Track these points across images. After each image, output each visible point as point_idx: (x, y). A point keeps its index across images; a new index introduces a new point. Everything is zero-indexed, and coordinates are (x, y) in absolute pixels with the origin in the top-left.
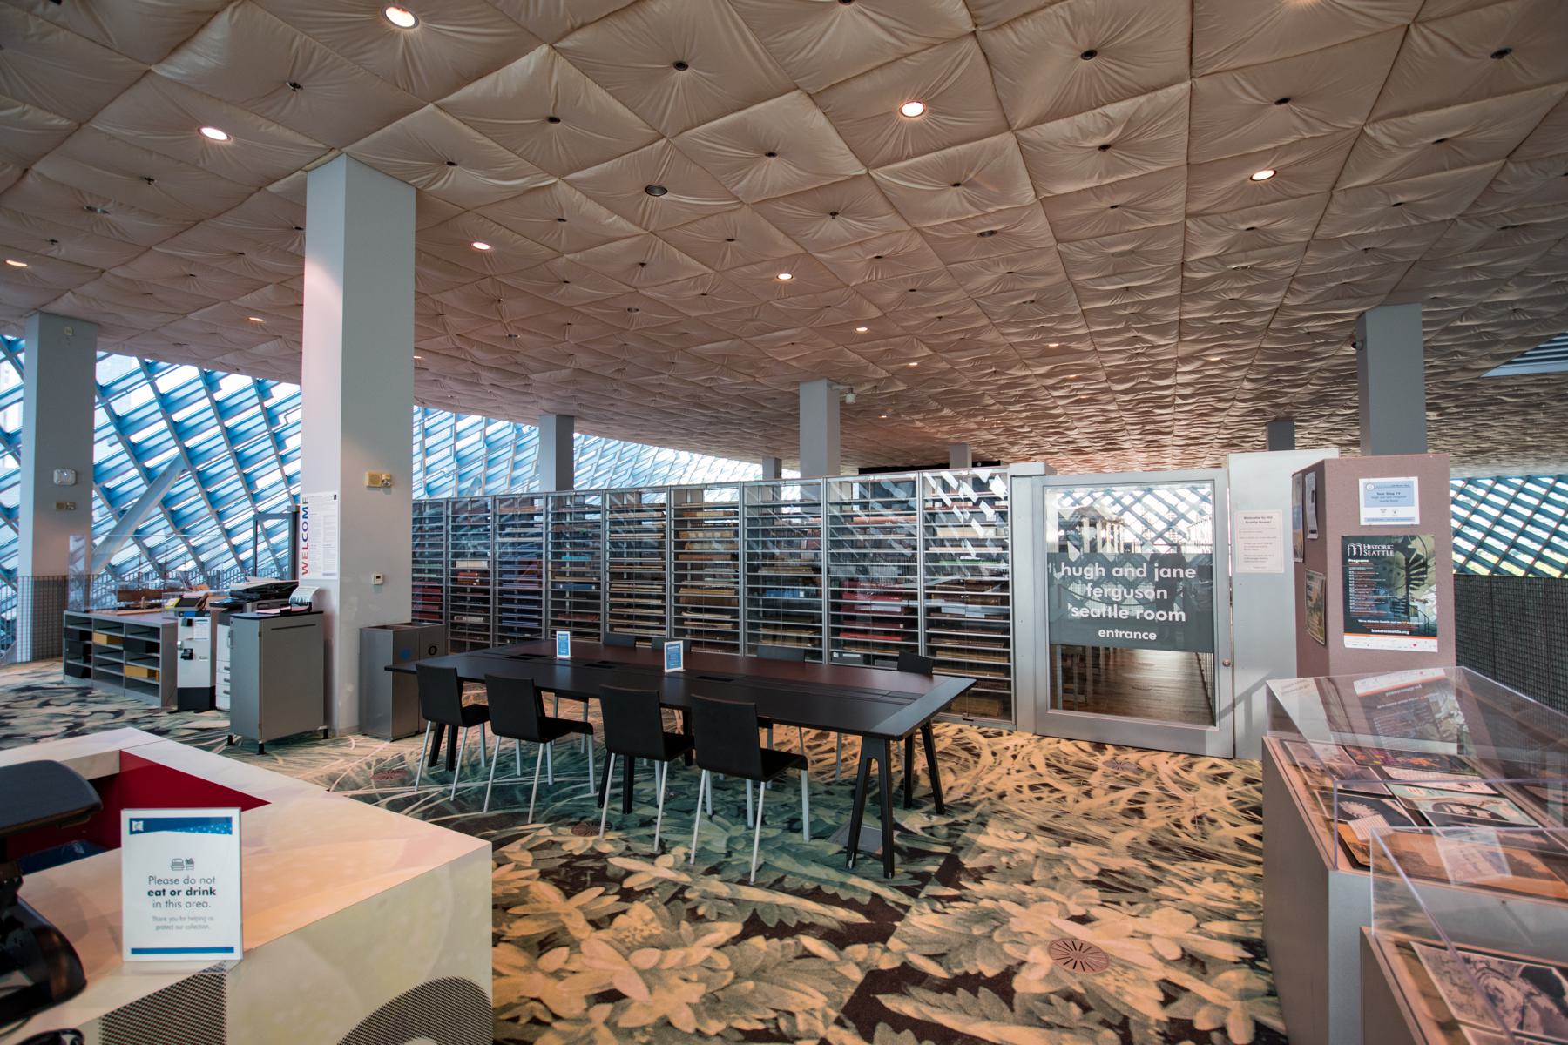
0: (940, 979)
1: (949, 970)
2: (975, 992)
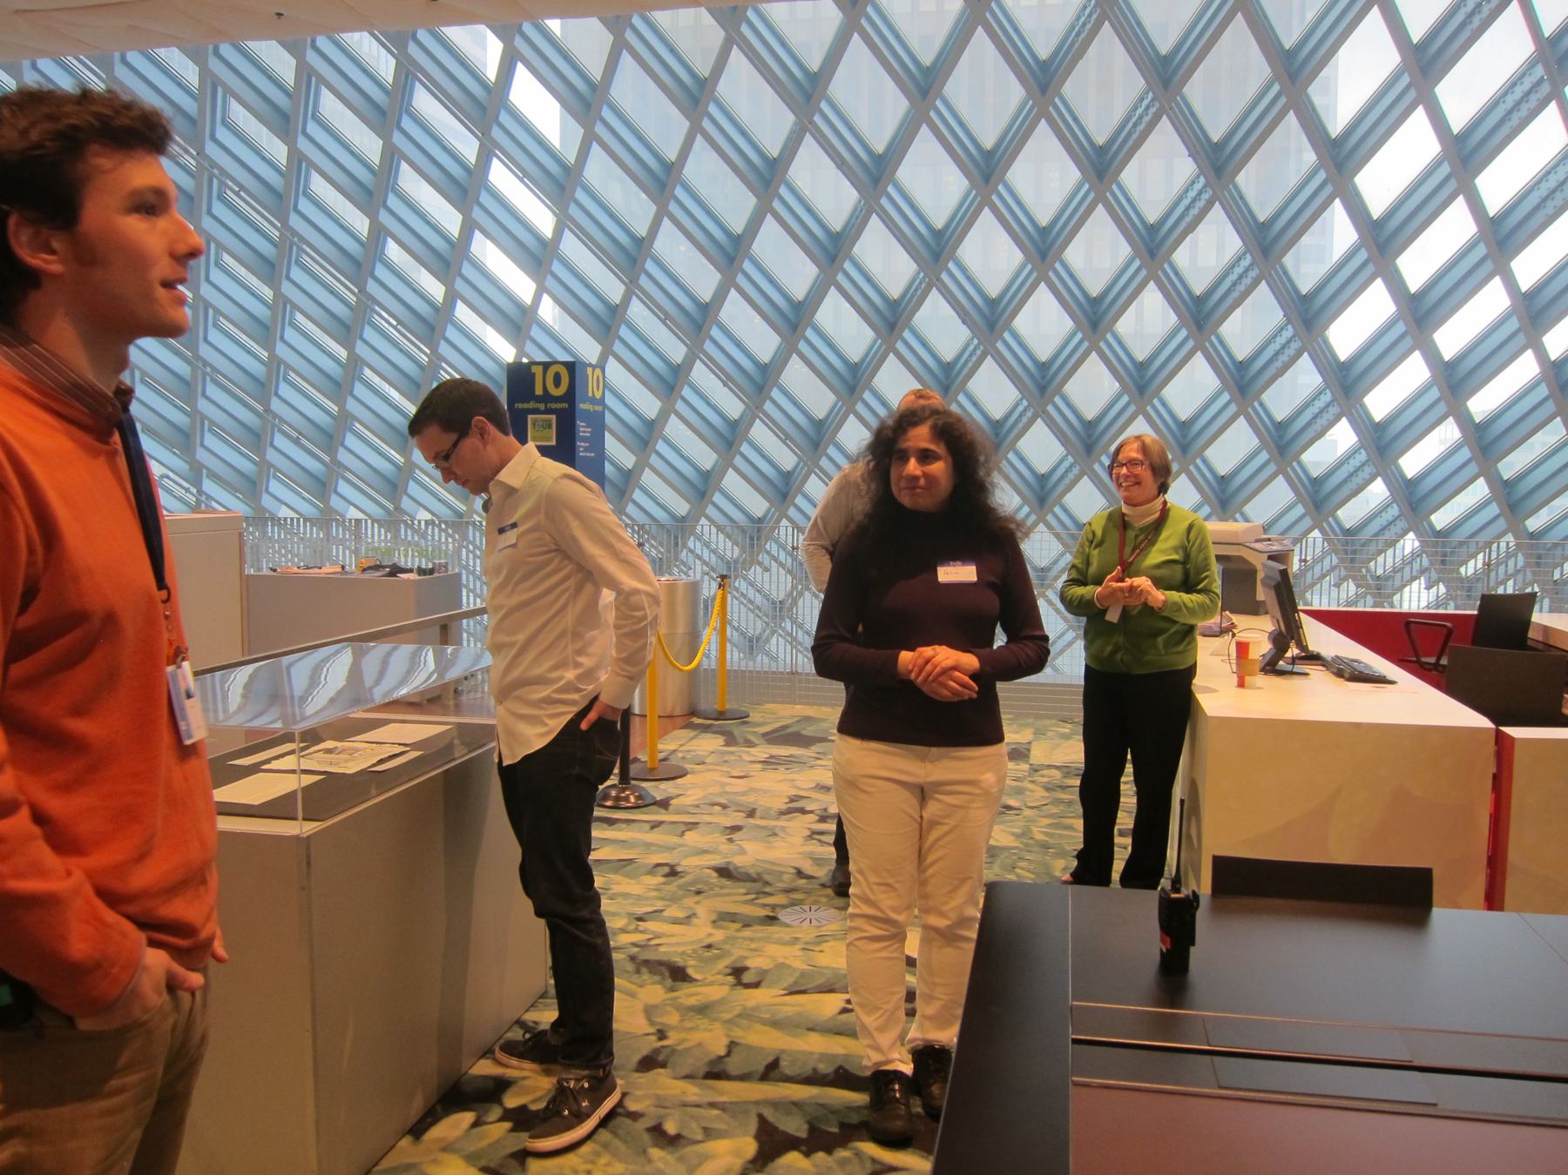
1: (858, 1154)
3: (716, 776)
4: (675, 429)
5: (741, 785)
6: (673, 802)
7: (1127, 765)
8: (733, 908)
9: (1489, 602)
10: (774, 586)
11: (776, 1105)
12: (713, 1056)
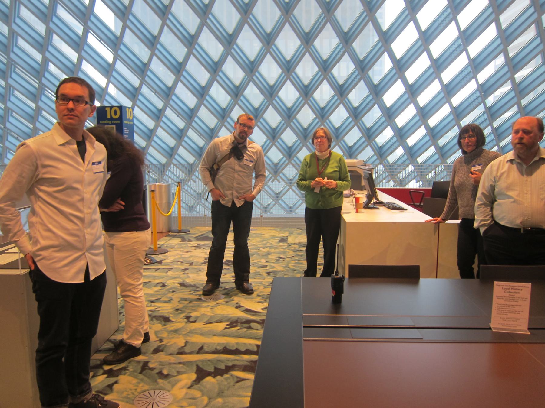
0: (235, 371)
1: (232, 376)
2: (216, 369)
3: (179, 252)
4: (160, 132)
5: (187, 255)
6: (163, 261)
7: (321, 243)
8: (186, 296)
9: (435, 184)
10: (197, 188)
11: (202, 361)
12: (180, 347)
